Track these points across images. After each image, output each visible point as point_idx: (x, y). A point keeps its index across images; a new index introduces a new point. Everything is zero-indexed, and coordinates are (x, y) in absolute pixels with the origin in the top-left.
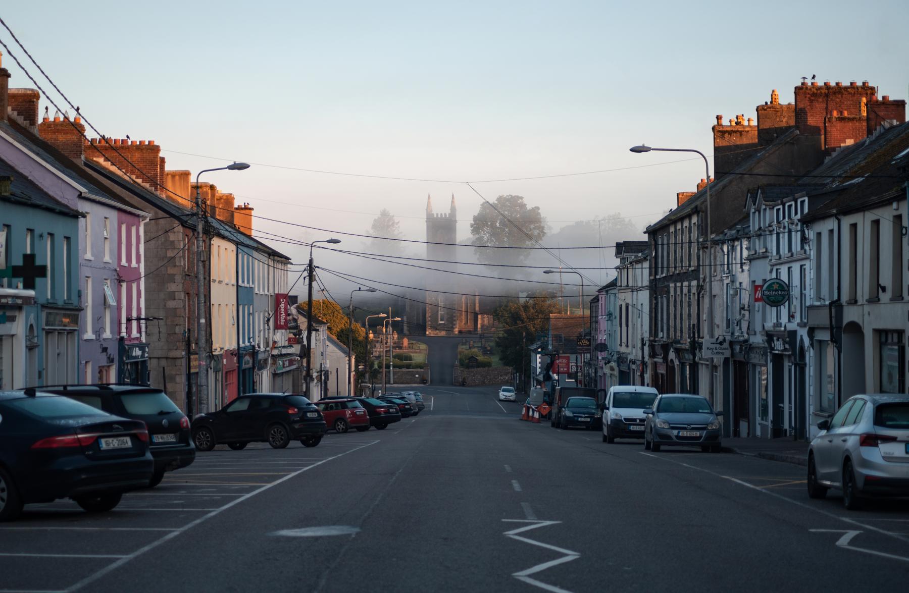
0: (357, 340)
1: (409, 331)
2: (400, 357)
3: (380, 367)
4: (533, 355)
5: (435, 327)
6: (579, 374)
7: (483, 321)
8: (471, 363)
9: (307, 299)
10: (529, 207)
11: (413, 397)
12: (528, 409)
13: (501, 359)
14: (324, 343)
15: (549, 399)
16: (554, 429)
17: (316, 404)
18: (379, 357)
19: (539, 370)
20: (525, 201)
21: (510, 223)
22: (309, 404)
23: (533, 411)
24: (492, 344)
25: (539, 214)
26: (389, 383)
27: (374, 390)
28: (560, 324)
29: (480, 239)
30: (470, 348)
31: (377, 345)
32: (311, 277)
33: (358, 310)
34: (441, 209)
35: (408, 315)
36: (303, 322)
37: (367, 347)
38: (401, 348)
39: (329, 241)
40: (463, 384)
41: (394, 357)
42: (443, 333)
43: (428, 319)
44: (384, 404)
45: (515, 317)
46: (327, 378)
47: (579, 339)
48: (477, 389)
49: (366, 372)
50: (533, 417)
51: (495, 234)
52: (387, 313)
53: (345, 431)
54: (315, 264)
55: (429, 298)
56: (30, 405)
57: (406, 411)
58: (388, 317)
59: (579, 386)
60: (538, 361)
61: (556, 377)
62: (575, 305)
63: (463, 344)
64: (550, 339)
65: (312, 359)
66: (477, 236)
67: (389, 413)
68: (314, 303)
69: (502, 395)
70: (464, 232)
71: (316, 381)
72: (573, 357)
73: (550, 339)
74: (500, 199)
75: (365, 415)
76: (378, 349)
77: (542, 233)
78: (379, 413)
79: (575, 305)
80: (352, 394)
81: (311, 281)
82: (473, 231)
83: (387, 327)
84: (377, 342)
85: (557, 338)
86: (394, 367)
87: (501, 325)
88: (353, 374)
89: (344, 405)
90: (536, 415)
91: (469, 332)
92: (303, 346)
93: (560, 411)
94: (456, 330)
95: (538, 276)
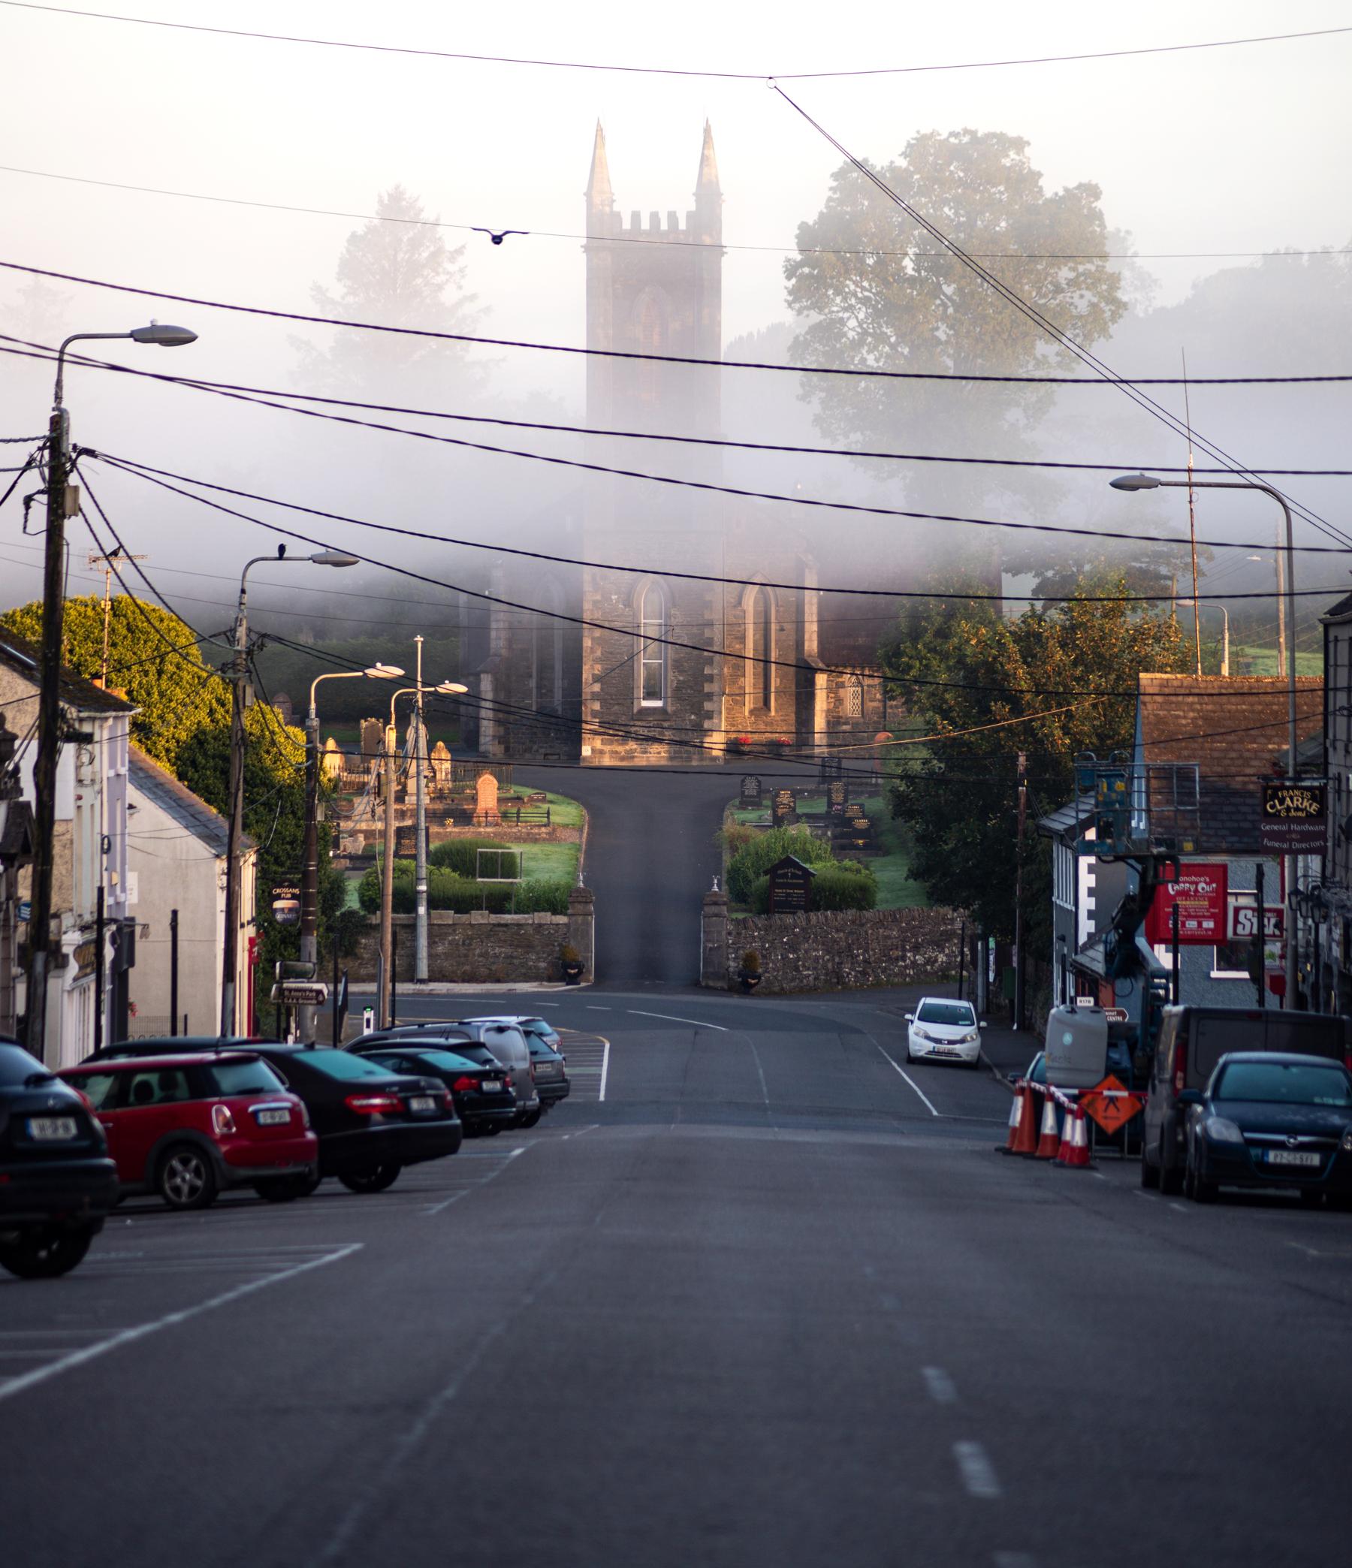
0: (268, 784)
1: (502, 740)
2: (458, 858)
3: (372, 903)
4: (1061, 856)
5: (617, 727)
6: (1273, 948)
7: (839, 699)
8: (780, 888)
9: (36, 594)
10: (1052, 186)
11: (516, 1043)
12: (1036, 1102)
13: (914, 874)
14: (117, 796)
15: (1132, 1055)
16: (1153, 1198)
17: (69, 1077)
18: (365, 860)
19: (1086, 927)
20: (1035, 158)
21: (961, 259)
22: (40, 1079)
23: (1061, 1111)
24: (878, 804)
25: (1098, 216)
26: (412, 978)
27: (340, 1009)
28: (1186, 717)
29: (828, 331)
30: (778, 821)
31: (361, 804)
32: (59, 499)
33: (271, 646)
34: (653, 191)
35: (505, 681)
36: (201, 759)
37: (311, 813)
38: (465, 818)
39: (141, 336)
40: (745, 983)
41: (437, 859)
42: (657, 755)
43: (590, 687)
44: (384, 1075)
45: (983, 685)
46: (126, 956)
47: (1271, 789)
48: (819, 1008)
49: (307, 928)
50: (1058, 1138)
51: (897, 304)
52: (404, 658)
53: (204, 1201)
54: (77, 435)
55: (596, 596)
56: (308, 1058)
57: (486, 1107)
58: (408, 680)
59: (1272, 1002)
60: (1083, 886)
61: (1163, 957)
62: (1255, 629)
63: (748, 802)
64: (1140, 785)
65: (58, 870)
66: (815, 317)
67: (407, 1114)
68: (71, 615)
69: (921, 1035)
70: (754, 301)
71: (73, 968)
72: (1241, 869)
73: (1140, 785)
74: (919, 148)
75: (295, 1125)
76: (362, 823)
77: (1110, 307)
78: (364, 1116)
79: (1255, 629)
80: (242, 1032)
81: (57, 516)
82: (796, 294)
83: (402, 725)
84: (361, 789)
85: (1174, 781)
86: (433, 904)
87: (918, 721)
88: (245, 934)
89: (201, 1079)
90: (1075, 1133)
91: (775, 749)
92: (18, 811)
93: (1181, 1114)
94: (716, 741)
95: (1087, 503)
